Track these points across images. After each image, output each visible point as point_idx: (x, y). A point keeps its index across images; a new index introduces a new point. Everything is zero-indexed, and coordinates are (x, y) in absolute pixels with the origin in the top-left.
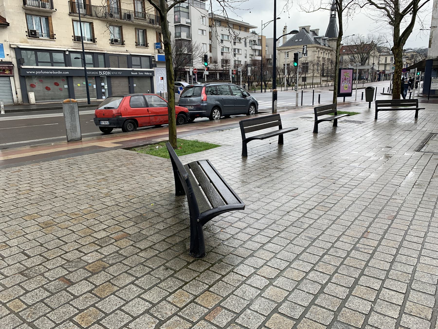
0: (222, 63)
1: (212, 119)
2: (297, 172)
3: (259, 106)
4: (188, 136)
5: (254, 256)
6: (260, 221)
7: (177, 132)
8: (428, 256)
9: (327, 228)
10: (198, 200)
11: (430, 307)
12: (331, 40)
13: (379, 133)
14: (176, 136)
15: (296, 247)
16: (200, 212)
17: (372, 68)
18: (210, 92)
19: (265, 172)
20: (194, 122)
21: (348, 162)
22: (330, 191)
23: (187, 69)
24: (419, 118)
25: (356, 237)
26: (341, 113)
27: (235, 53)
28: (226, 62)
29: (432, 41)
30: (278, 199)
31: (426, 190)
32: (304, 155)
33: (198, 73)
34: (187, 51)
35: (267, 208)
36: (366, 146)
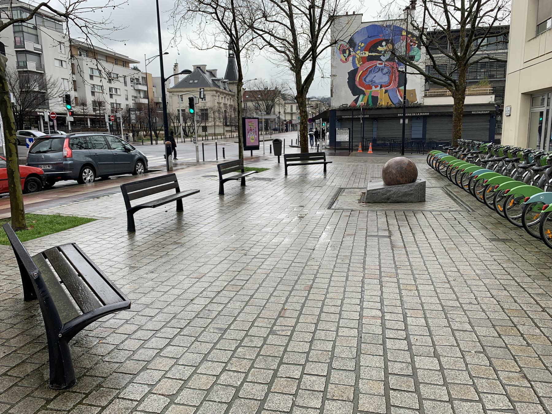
0: (93, 106)
1: (81, 181)
2: (202, 246)
3: (149, 162)
4: (45, 208)
5: (148, 369)
6: (156, 318)
7: (25, 203)
8: (346, 326)
9: (239, 313)
10: (58, 305)
11: (352, 386)
12: (232, 83)
13: (290, 191)
14: (23, 211)
15: (203, 344)
16: (63, 322)
17: (279, 118)
18: (77, 144)
19: (161, 250)
20: (55, 188)
21: (260, 227)
22: (242, 265)
23: (39, 112)
24: (327, 172)
25: (272, 318)
26: (249, 169)
27: (111, 93)
28: (98, 104)
29: (334, 91)
30: (178, 284)
31: (339, 251)
32: (209, 223)
33: (58, 119)
34: (37, 88)
35: (164, 300)
36: (278, 206)
